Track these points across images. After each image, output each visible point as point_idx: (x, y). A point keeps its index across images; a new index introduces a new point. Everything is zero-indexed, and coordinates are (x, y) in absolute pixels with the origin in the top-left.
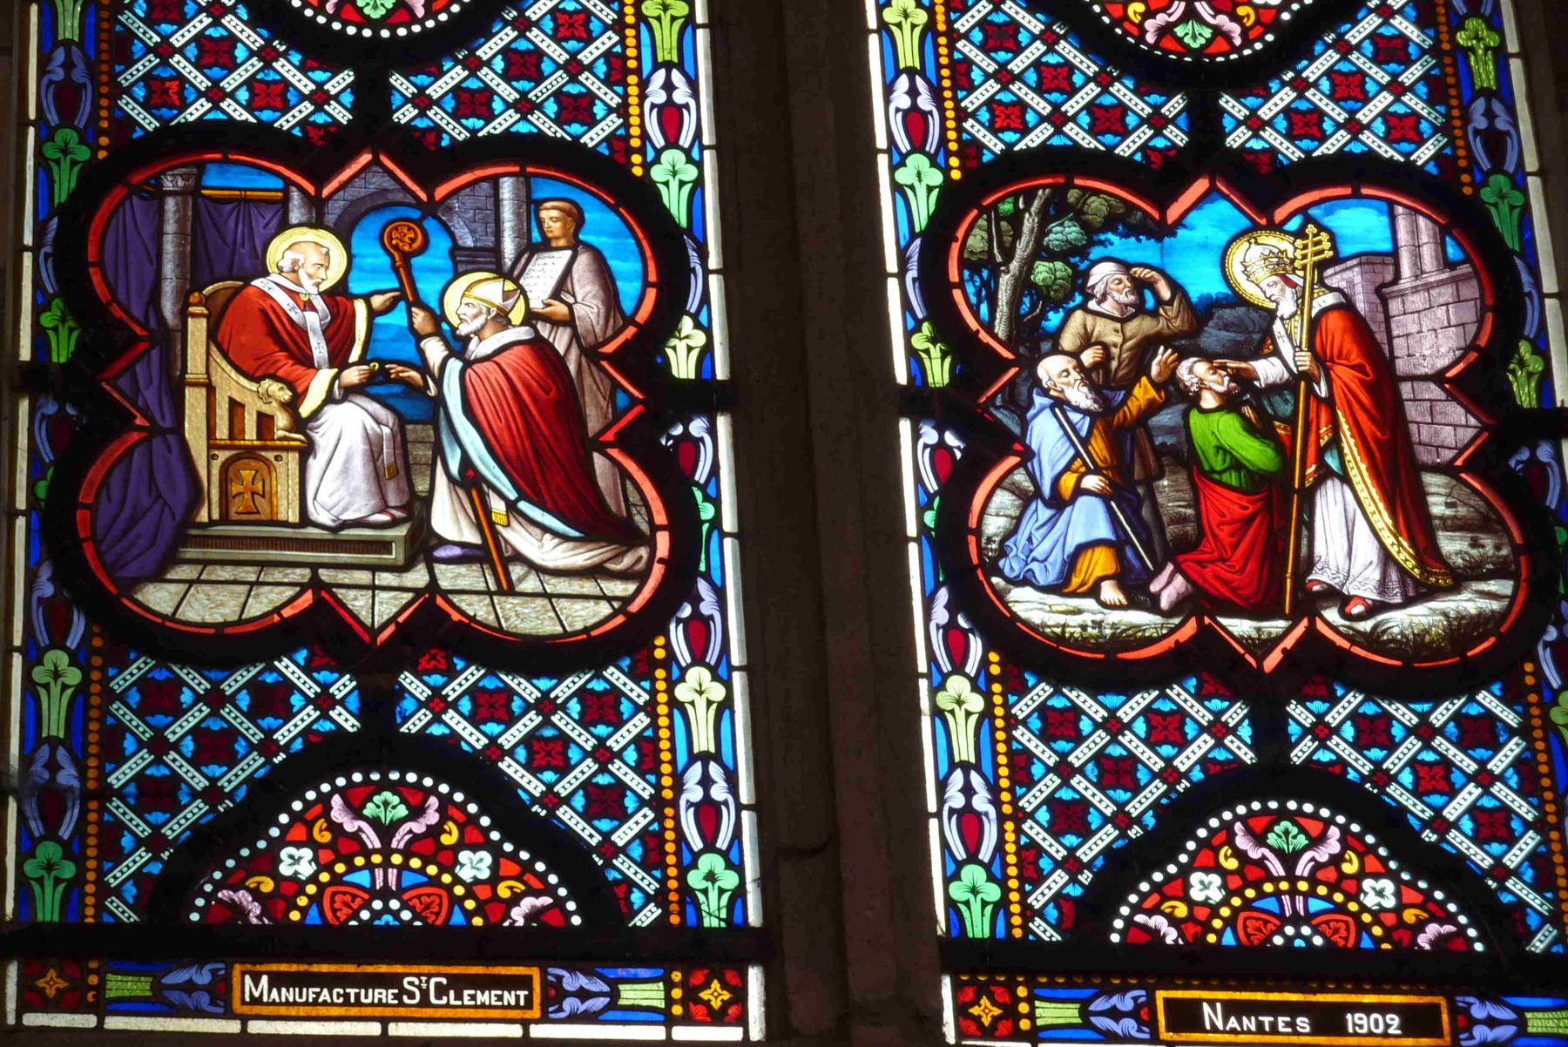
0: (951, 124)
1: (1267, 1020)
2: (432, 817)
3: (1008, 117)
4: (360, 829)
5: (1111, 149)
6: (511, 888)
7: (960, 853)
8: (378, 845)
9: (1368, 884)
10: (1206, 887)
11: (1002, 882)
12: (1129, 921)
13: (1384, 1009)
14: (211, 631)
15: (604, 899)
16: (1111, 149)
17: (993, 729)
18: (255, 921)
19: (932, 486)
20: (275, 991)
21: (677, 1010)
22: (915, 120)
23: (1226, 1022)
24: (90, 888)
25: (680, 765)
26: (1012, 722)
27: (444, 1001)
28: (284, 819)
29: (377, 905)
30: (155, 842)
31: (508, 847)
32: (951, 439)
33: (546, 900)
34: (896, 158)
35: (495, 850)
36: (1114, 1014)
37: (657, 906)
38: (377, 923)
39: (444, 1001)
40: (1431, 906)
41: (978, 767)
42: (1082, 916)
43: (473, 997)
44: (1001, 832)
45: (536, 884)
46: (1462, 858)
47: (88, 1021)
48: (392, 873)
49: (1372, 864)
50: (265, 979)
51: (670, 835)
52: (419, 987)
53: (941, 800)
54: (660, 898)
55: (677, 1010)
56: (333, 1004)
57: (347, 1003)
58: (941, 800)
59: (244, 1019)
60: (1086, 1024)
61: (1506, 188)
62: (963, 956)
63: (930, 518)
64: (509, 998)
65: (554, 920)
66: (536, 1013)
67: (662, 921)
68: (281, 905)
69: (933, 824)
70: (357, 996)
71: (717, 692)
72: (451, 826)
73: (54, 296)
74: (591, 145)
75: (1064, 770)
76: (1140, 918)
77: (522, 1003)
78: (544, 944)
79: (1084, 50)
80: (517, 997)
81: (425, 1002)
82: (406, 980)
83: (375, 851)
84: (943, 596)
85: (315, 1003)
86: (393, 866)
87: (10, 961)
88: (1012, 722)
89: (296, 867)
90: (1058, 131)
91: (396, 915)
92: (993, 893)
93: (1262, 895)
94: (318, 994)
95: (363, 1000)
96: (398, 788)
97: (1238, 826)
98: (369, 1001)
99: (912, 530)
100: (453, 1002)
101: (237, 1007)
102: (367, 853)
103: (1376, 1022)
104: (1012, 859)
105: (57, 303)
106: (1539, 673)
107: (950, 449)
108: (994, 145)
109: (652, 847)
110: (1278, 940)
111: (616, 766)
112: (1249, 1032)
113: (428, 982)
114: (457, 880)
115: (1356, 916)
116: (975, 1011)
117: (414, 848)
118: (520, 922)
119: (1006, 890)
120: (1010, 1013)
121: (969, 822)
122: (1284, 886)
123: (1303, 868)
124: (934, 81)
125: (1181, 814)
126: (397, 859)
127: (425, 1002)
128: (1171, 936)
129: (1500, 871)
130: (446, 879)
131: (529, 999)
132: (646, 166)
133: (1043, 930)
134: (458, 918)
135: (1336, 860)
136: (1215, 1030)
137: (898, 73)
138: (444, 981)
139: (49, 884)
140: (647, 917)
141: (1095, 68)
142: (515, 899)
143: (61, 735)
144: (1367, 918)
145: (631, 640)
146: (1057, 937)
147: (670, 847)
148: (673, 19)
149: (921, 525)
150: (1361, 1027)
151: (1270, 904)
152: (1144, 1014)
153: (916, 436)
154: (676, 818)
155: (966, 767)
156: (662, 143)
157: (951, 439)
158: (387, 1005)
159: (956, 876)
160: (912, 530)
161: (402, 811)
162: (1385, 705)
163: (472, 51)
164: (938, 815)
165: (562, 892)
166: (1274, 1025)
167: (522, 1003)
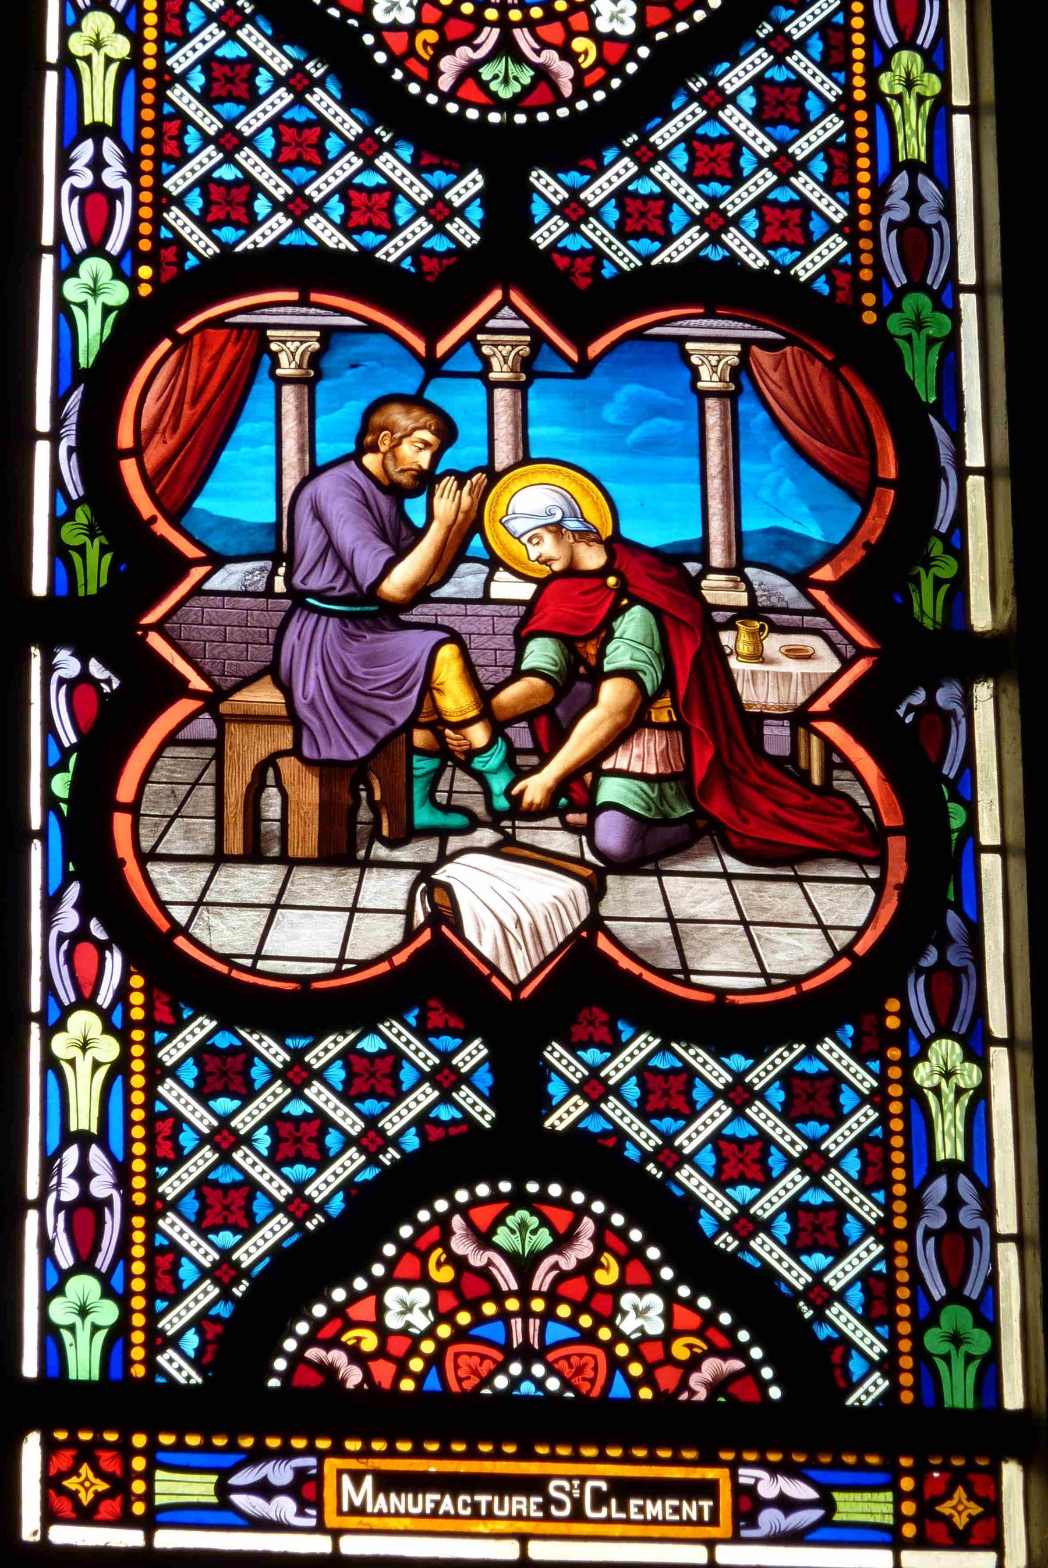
2: (584, 1249)
4: (490, 1262)
6: (690, 1346)
8: (514, 1286)
9: (628, 1300)
10: (407, 1307)
11: (123, 1300)
12: (296, 1359)
17: (128, 1090)
19: (68, 736)
20: (381, 1497)
21: (909, 1530)
24: (138, 1337)
25: (917, 1181)
26: (156, 1072)
27: (603, 1513)
28: (389, 1250)
31: (684, 1291)
32: (96, 669)
33: (737, 1365)
34: (65, 261)
35: (667, 1291)
36: (265, 1490)
37: (884, 1376)
39: (603, 1513)
40: (712, 1333)
41: (102, 1139)
43: (642, 1510)
45: (722, 1342)
46: (768, 1273)
47: (132, 1538)
48: (534, 1324)
49: (638, 1274)
50: (368, 1481)
51: (903, 1277)
52: (570, 1494)
54: (888, 1366)
55: (909, 1530)
56: (457, 1516)
57: (476, 1515)
59: (336, 1534)
60: (225, 1504)
62: (56, 1401)
63: (61, 785)
64: (689, 1510)
65: (746, 1393)
66: (725, 1528)
67: (892, 1394)
70: (490, 1505)
71: (969, 1076)
72: (607, 1258)
74: (804, 277)
75: (815, 1163)
76: (313, 1353)
77: (706, 1518)
78: (725, 1426)
80: (700, 1510)
81: (578, 1515)
82: (553, 1484)
83: (510, 1294)
84: (74, 891)
85: (434, 1514)
89: (409, 1317)
90: (298, 224)
91: (540, 1383)
92: (108, 1313)
93: (479, 1319)
94: (438, 1504)
95: (497, 1511)
97: (457, 1221)
98: (505, 1513)
100: (615, 1515)
101: (332, 1520)
102: (499, 1296)
104: (138, 1268)
105: (82, 515)
107: (96, 683)
108: (203, 245)
109: (877, 1296)
110: (486, 1391)
111: (833, 1179)
113: (582, 1488)
114: (619, 1336)
115: (608, 1347)
116: (71, 1483)
118: (702, 1395)
120: (120, 1485)
121: (85, 1214)
122: (512, 1305)
123: (542, 1280)
124: (130, 145)
127: (578, 1515)
128: (354, 1377)
129: (820, 1294)
130: (605, 1334)
131: (715, 1511)
132: (882, 311)
133: (178, 1368)
134: (620, 1390)
135: (588, 1267)
137: (896, 167)
138: (604, 1486)
140: (871, 1389)
142: (694, 1363)
144: (622, 1350)
145: (853, 997)
146: (196, 1379)
151: (494, 1332)
152: (746, 1504)
154: (911, 1254)
155: (84, 1140)
157: (96, 669)
158: (529, 1518)
159: (59, 1290)
163: (645, 136)
164: (40, 1204)
165: (756, 1353)
167: (706, 1518)
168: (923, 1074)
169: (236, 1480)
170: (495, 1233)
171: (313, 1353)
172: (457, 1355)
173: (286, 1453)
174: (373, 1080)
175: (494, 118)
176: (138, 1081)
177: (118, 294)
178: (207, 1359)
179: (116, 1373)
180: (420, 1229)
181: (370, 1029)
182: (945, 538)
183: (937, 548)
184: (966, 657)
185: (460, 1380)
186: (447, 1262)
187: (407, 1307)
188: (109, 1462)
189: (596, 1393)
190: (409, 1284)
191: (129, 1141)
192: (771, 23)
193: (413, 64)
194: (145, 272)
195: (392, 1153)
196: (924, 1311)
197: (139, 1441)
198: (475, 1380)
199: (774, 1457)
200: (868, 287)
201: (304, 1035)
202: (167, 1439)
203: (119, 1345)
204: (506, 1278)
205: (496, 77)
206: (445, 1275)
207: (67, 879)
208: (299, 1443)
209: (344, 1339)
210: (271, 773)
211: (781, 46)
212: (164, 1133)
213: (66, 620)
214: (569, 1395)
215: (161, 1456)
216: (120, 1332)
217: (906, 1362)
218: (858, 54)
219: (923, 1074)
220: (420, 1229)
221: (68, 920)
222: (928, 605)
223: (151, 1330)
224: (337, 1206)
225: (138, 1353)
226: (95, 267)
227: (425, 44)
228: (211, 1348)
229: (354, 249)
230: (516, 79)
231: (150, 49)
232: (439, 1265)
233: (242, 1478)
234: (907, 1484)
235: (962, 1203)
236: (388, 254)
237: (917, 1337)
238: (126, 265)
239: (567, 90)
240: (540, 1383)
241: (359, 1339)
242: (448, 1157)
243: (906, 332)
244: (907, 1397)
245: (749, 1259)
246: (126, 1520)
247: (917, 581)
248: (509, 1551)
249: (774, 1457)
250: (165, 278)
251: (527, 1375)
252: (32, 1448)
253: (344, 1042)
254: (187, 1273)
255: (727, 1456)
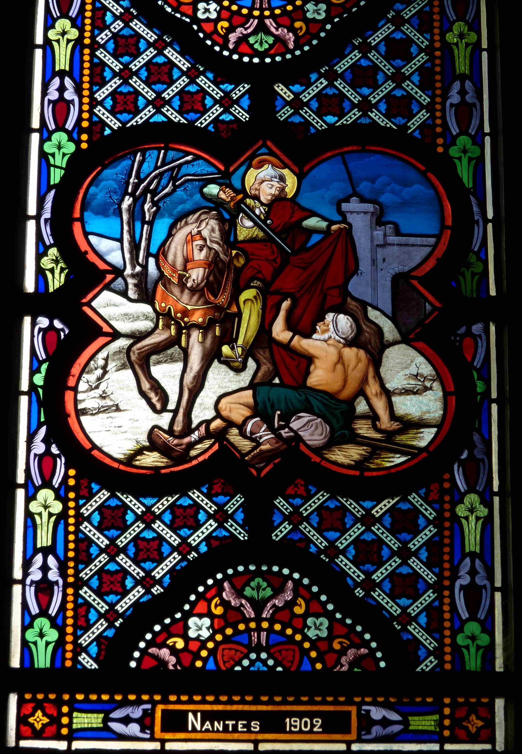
0: (86, 107)
1: (230, 723)
3: (125, 103)
5: (191, 123)
7: (34, 609)
13: (312, 715)
14: (148, 472)
15: (404, 651)
16: (191, 123)
17: (67, 525)
18: (171, 668)
22: (61, 107)
23: (202, 725)
24: (69, 647)
26: (80, 519)
29: (253, 656)
30: (110, 615)
32: (57, 324)
34: (46, 134)
38: (252, 669)
42: (113, 650)
44: (65, 595)
45: (357, 641)
47: (62, 745)
48: (264, 635)
51: (446, 608)
53: (26, 574)
58: (26, 574)
61: (469, 145)
62: (28, 679)
63: (39, 380)
68: (190, 657)
69: (17, 589)
72: (300, 601)
73: (51, 246)
76: (152, 650)
78: (364, 683)
79: (182, 53)
84: (43, 431)
86: (264, 630)
87: (260, 698)
88: (80, 519)
89: (200, 632)
96: (267, 576)
99: (24, 386)
103: (306, 723)
104: (70, 613)
105: (53, 252)
106: (453, 480)
110: (238, 668)
112: (218, 731)
117: (277, 617)
119: (62, 634)
120: (55, 719)
121: (44, 588)
122: (253, 625)
125: (183, 581)
126: (265, 625)
129: (406, 618)
130: (298, 637)
133: (87, 662)
134: (306, 666)
136: (194, 730)
139: (473, 650)
140: (428, 664)
141: (188, 65)
142: (343, 652)
143: (478, 551)
146: (95, 666)
147: (447, 616)
148: (69, 41)
149: (32, 385)
150: (295, 727)
153: (34, 324)
156: (54, 127)
157: (57, 324)
159: (31, 626)
160: (24, 386)
161: (269, 592)
162: (343, 501)
165: (374, 645)
166: (235, 727)
168: (461, 511)
169: (113, 715)
170: (245, 590)
171: (152, 650)
172: (223, 650)
173: (139, 702)
174: (185, 519)
175: (256, 60)
176: (72, 521)
177: (71, 148)
178: (101, 658)
179: (58, 664)
180: (208, 588)
181: (184, 494)
182: (477, 254)
183: (473, 258)
184: (484, 309)
185: (224, 662)
186: (220, 605)
187: (199, 627)
188: (52, 710)
189: (293, 669)
190: (201, 616)
191: (67, 550)
192: (394, 11)
193: (215, 37)
194: (84, 137)
195: (194, 554)
196: (457, 625)
197: (66, 697)
198: (232, 663)
199: (381, 699)
200: (440, 135)
201: (153, 496)
202: (80, 697)
203: (60, 651)
204: (249, 612)
205: (256, 42)
206: (219, 611)
207: (40, 425)
208: (145, 697)
209: (168, 642)
210: (159, 164)
211: (398, 22)
212: (84, 550)
213: (42, 302)
214: (279, 669)
215: (77, 705)
216: (60, 643)
217: (448, 649)
218: (436, 24)
219: (461, 511)
220: (208, 588)
221: (39, 448)
222: (468, 286)
223: (75, 643)
224: (167, 580)
225: (69, 655)
226: (60, 137)
227: (222, 28)
228: (103, 653)
229: (186, 122)
230: (266, 42)
231: (87, 34)
232: (216, 606)
233: (116, 715)
234: (447, 711)
235: (478, 573)
236: (201, 123)
237: (453, 637)
238: (75, 135)
239: (291, 46)
240: (264, 662)
241: (175, 643)
242: (221, 552)
243: (56, 38)
244: (448, 666)
245: (370, 601)
246: (59, 737)
247: (463, 275)
248: (249, 747)
249: (381, 699)
250: (95, 139)
251: (258, 659)
252: (13, 699)
253: (171, 500)
254: (93, 616)
255: (357, 699)
